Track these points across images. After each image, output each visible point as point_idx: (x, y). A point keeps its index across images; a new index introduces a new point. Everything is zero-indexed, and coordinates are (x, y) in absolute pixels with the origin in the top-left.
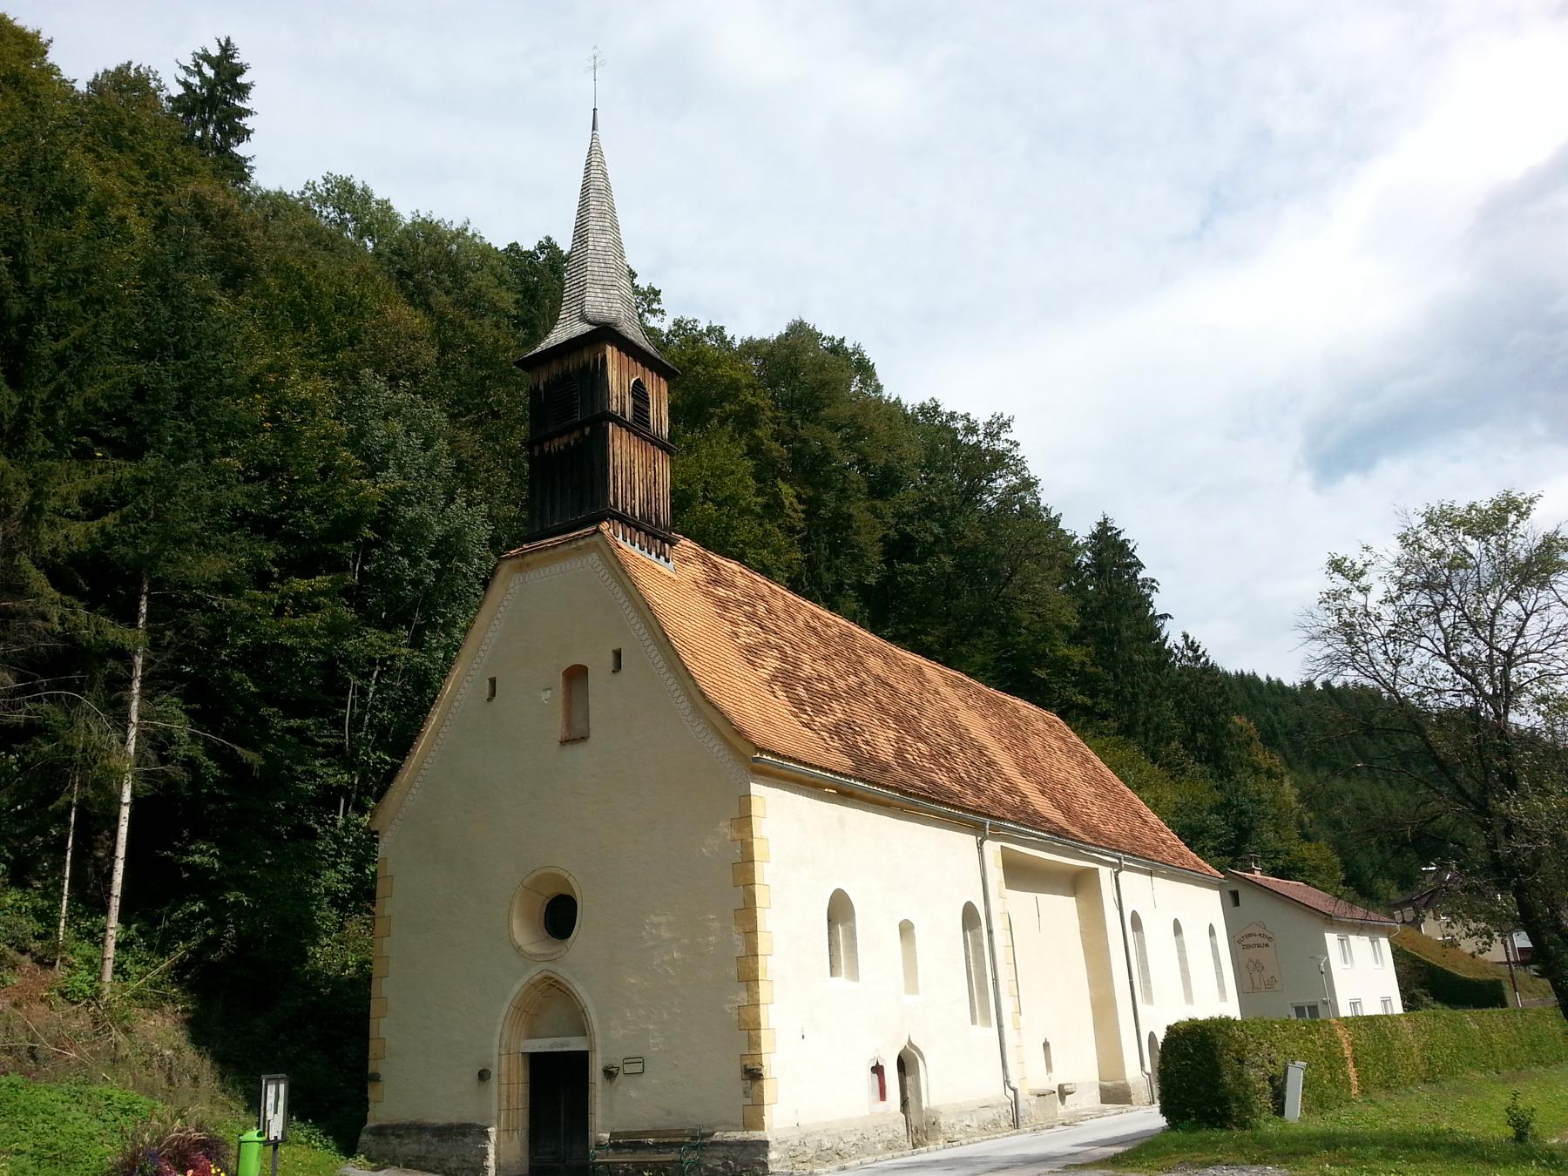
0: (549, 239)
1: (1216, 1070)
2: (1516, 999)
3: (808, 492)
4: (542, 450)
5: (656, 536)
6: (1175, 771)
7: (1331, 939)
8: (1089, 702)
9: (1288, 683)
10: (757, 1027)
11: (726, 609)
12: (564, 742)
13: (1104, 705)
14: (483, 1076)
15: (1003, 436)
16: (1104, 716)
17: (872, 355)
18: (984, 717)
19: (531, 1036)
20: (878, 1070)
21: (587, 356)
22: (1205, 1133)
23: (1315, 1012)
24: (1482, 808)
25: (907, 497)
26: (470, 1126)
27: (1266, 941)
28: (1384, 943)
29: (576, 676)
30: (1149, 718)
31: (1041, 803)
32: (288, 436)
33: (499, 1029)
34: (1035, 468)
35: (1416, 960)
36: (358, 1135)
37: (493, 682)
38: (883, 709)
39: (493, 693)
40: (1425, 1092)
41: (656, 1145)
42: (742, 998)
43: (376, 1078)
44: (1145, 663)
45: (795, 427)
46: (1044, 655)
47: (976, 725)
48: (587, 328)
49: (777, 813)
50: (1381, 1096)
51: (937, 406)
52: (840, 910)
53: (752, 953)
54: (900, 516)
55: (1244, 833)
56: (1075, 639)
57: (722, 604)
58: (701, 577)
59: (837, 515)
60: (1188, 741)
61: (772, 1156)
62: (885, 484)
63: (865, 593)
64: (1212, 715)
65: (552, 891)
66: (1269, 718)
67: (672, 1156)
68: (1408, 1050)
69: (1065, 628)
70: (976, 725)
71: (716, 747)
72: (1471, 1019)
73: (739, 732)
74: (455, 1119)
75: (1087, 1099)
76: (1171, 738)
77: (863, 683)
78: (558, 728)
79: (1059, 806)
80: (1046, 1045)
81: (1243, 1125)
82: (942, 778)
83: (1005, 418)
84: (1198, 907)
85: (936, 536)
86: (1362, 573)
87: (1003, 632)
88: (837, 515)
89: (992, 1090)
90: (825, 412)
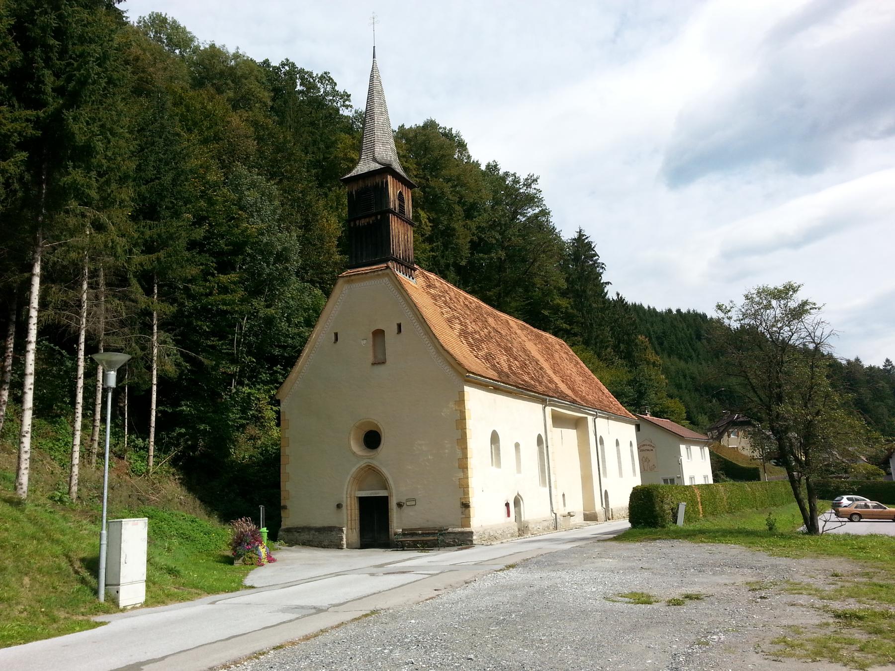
0: (287, 60)
1: (653, 505)
2: (765, 477)
3: (433, 215)
4: (355, 224)
5: (408, 267)
6: (609, 363)
7: (683, 448)
8: (568, 327)
9: (658, 310)
10: (468, 487)
11: (436, 300)
12: (373, 364)
13: (576, 329)
14: (339, 506)
15: (533, 186)
16: (575, 335)
17: (466, 138)
18: (535, 344)
19: (360, 490)
20: (507, 505)
21: (378, 180)
22: (646, 530)
23: (674, 480)
24: (769, 408)
25: (481, 219)
26: (335, 527)
27: (650, 448)
28: (707, 450)
29: (379, 334)
30: (598, 336)
31: (563, 387)
32: (211, 202)
33: (346, 487)
34: (549, 202)
35: (719, 457)
36: (277, 532)
37: (336, 335)
38: (499, 345)
39: (336, 339)
40: (728, 517)
41: (422, 534)
42: (461, 475)
43: (285, 507)
44: (597, 308)
45: (428, 180)
46: (548, 303)
47: (533, 349)
48: (378, 166)
49: (474, 397)
50: (711, 518)
51: (497, 165)
52: (495, 438)
53: (465, 457)
54: (478, 228)
55: (641, 395)
56: (563, 294)
57: (434, 297)
58: (424, 284)
59: (448, 227)
60: (616, 348)
61: (474, 537)
62: (470, 211)
63: (459, 270)
64: (628, 334)
65: (368, 429)
66: (648, 329)
67: (431, 538)
68: (721, 499)
69: (559, 289)
70: (533, 349)
71: (448, 370)
72: (747, 486)
73: (460, 364)
74: (326, 525)
75: (579, 519)
76: (607, 347)
77: (490, 332)
78: (370, 358)
79: (569, 388)
80: (564, 495)
81: (663, 527)
82: (526, 378)
83: (535, 177)
84: (626, 433)
85: (497, 240)
86: (729, 311)
87: (527, 290)
88: (448, 227)
89: (547, 514)
90: (443, 172)
